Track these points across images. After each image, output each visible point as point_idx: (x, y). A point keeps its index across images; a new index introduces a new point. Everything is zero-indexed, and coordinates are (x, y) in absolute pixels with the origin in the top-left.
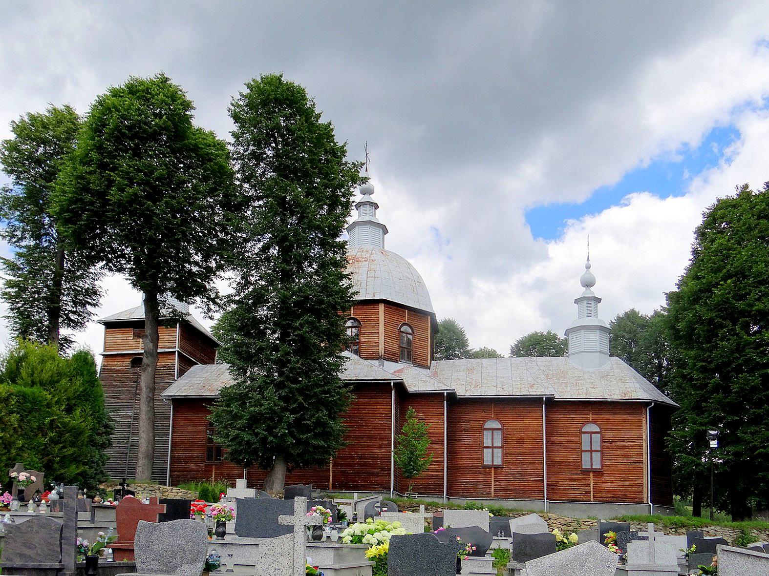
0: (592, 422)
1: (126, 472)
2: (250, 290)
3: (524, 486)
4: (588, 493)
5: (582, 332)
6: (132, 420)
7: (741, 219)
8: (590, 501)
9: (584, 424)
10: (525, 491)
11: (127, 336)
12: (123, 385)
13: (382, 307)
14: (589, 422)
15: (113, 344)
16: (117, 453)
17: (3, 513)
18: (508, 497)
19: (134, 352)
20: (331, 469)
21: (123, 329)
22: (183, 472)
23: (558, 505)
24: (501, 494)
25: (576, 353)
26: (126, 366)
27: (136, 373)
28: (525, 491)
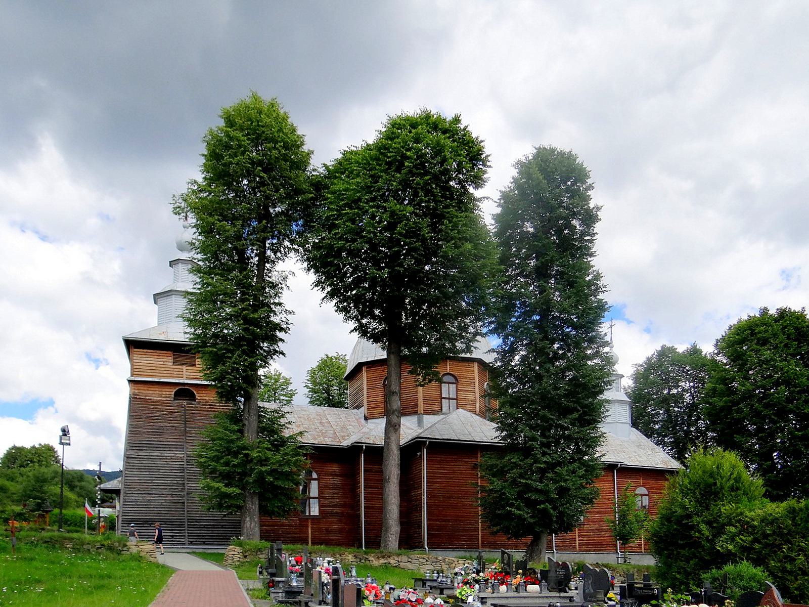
0: (643, 486)
1: (186, 526)
2: (517, 358)
3: (602, 540)
4: (640, 545)
5: (450, 376)
6: (185, 463)
7: (352, 239)
8: (641, 552)
9: (637, 487)
10: (601, 545)
11: (166, 361)
12: (164, 419)
13: (476, 365)
14: (640, 486)
15: (144, 368)
16: (170, 503)
17: (349, 598)
18: (589, 550)
19: (177, 381)
20: (480, 529)
21: (158, 351)
22: (274, 526)
23: (644, 556)
24: (584, 548)
25: (612, 423)
26: (166, 397)
27: (182, 407)
28: (601, 545)
